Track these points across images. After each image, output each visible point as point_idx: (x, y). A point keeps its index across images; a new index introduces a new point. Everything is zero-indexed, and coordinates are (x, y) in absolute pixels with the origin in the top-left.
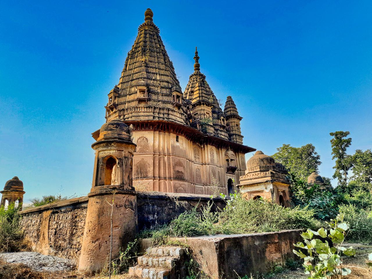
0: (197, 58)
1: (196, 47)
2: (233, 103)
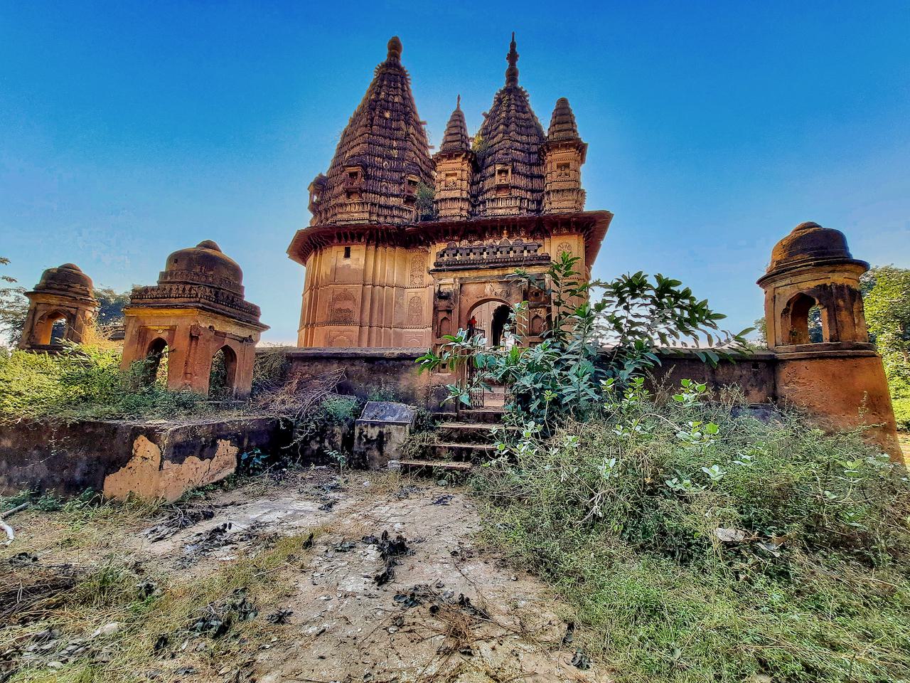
0: (513, 57)
1: (513, 33)
2: (569, 114)
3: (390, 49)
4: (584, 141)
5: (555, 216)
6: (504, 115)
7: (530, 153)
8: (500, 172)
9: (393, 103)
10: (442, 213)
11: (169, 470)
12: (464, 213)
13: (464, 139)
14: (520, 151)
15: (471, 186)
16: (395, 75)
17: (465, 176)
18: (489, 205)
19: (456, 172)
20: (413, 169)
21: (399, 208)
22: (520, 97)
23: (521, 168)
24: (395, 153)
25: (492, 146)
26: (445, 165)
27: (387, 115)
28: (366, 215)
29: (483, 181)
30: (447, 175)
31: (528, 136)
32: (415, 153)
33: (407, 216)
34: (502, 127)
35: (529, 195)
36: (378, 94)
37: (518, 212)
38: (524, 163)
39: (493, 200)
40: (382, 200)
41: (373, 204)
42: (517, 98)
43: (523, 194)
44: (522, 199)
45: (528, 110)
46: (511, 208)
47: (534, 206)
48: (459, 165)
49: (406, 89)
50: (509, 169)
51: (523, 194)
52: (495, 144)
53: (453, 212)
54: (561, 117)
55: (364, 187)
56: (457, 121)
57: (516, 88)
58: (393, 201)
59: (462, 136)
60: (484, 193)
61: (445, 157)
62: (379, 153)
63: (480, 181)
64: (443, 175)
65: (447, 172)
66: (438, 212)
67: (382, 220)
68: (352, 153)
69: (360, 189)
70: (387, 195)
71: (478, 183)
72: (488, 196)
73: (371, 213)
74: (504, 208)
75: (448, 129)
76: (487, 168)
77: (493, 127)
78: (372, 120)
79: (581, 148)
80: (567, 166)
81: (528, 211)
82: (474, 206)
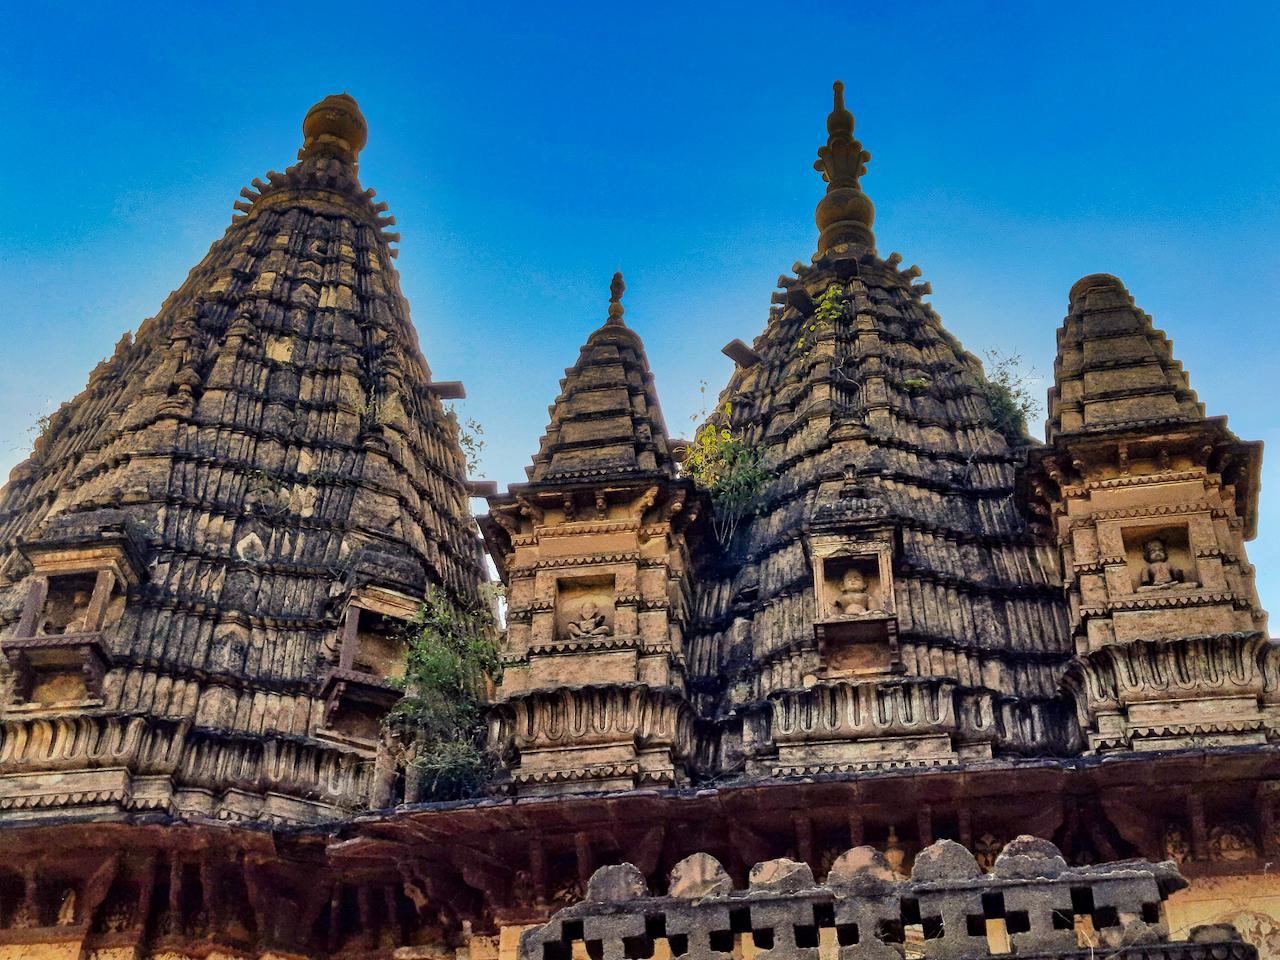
2: (1140, 328)
3: (313, 130)
4: (1241, 430)
5: (1176, 769)
6: (827, 349)
7: (972, 496)
8: (836, 569)
9: (312, 311)
10: (535, 764)
11: (763, 733)
12: (657, 765)
13: (645, 432)
14: (921, 483)
15: (686, 639)
16: (328, 217)
17: (656, 586)
18: (786, 722)
19: (611, 569)
20: (389, 565)
21: (299, 749)
22: (890, 291)
23: (934, 552)
24: (302, 500)
25: (784, 467)
26: (555, 542)
27: (280, 351)
28: (111, 783)
29: (749, 615)
30: (563, 586)
31: (950, 428)
32: (403, 502)
33: (336, 786)
34: (821, 393)
35: (994, 676)
36: (246, 278)
37: (947, 756)
38: (949, 535)
39: (808, 699)
40: (214, 708)
41: (157, 727)
42: (880, 294)
43: (964, 668)
44: (960, 695)
45: (933, 335)
46: (912, 737)
47: (1032, 730)
48: (627, 542)
49: (375, 265)
50: (880, 549)
51: (964, 668)
52: (799, 458)
53: (597, 758)
54: (1105, 346)
55: (117, 643)
56: (614, 362)
57: (869, 259)
58: (267, 711)
59: (636, 422)
60: (759, 670)
61: (553, 505)
62: (223, 497)
63: (732, 614)
64: (543, 588)
65: (566, 573)
66: (514, 756)
67: (194, 804)
68: (81, 495)
69: (97, 649)
70: (241, 685)
71: (723, 624)
72: (781, 677)
73: (136, 772)
74: (865, 736)
75: (569, 398)
76: (763, 556)
77: (781, 398)
78: (204, 368)
79: (1231, 464)
80: (1175, 539)
81: (999, 751)
82: (707, 732)
